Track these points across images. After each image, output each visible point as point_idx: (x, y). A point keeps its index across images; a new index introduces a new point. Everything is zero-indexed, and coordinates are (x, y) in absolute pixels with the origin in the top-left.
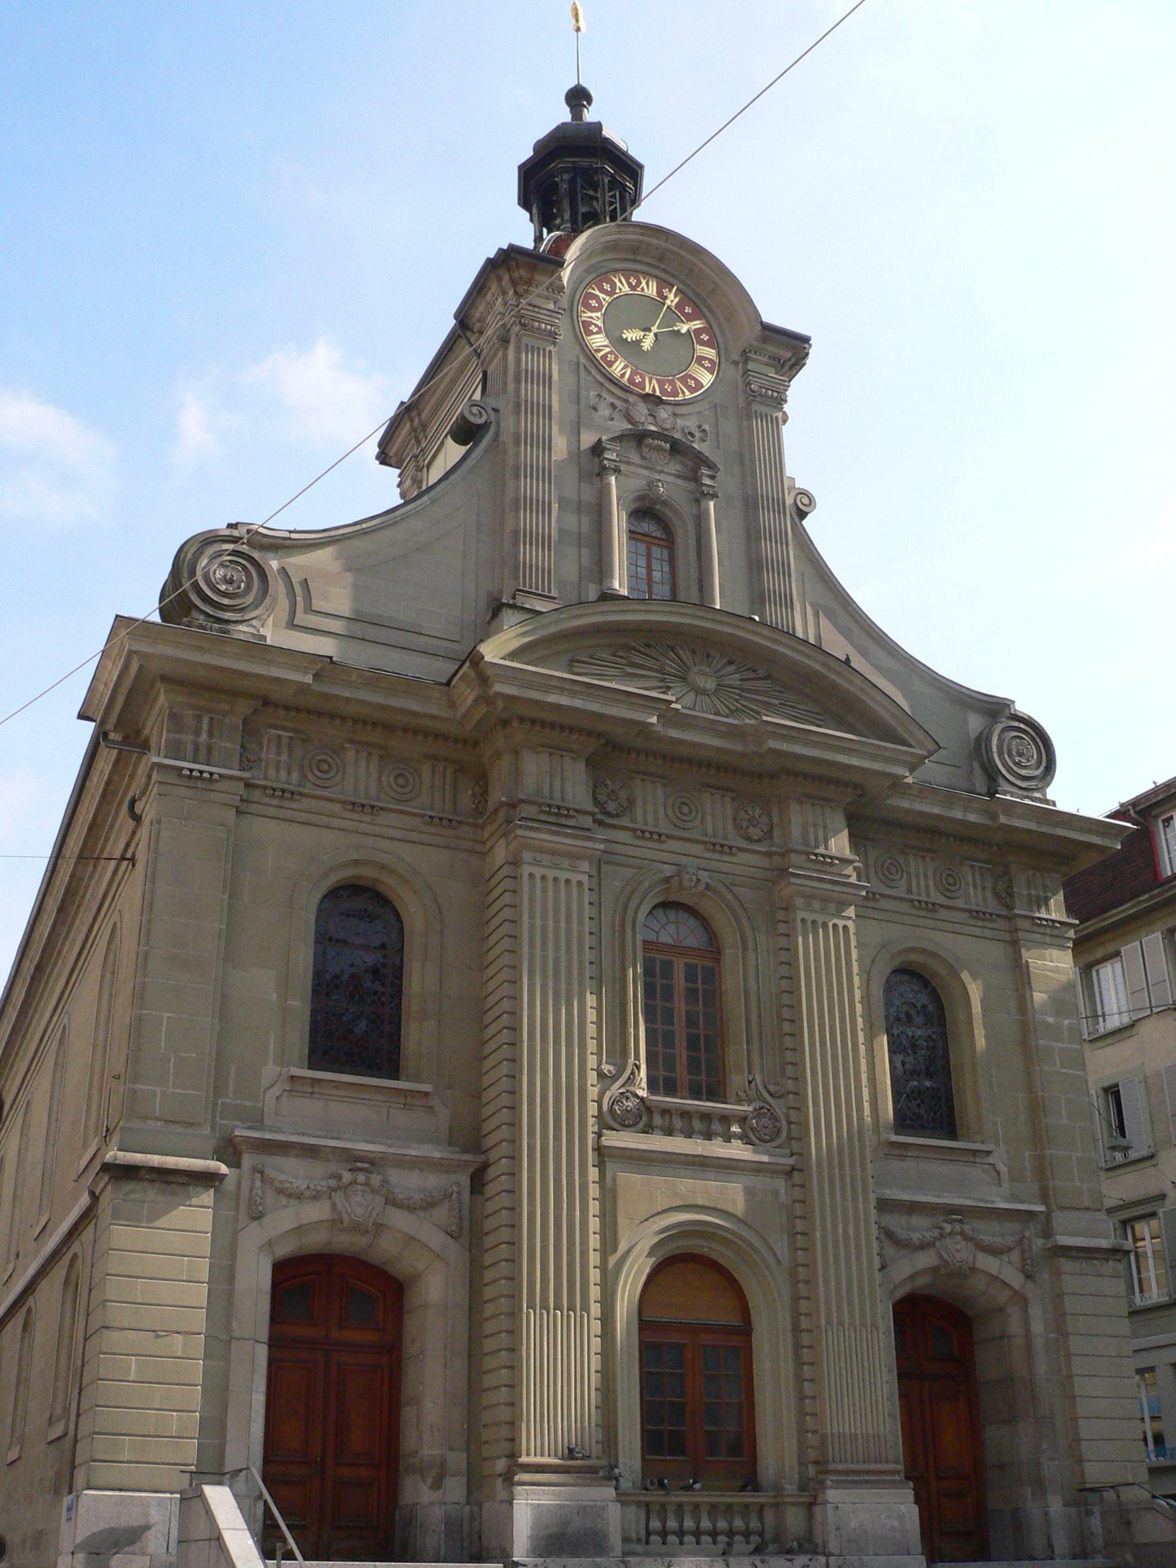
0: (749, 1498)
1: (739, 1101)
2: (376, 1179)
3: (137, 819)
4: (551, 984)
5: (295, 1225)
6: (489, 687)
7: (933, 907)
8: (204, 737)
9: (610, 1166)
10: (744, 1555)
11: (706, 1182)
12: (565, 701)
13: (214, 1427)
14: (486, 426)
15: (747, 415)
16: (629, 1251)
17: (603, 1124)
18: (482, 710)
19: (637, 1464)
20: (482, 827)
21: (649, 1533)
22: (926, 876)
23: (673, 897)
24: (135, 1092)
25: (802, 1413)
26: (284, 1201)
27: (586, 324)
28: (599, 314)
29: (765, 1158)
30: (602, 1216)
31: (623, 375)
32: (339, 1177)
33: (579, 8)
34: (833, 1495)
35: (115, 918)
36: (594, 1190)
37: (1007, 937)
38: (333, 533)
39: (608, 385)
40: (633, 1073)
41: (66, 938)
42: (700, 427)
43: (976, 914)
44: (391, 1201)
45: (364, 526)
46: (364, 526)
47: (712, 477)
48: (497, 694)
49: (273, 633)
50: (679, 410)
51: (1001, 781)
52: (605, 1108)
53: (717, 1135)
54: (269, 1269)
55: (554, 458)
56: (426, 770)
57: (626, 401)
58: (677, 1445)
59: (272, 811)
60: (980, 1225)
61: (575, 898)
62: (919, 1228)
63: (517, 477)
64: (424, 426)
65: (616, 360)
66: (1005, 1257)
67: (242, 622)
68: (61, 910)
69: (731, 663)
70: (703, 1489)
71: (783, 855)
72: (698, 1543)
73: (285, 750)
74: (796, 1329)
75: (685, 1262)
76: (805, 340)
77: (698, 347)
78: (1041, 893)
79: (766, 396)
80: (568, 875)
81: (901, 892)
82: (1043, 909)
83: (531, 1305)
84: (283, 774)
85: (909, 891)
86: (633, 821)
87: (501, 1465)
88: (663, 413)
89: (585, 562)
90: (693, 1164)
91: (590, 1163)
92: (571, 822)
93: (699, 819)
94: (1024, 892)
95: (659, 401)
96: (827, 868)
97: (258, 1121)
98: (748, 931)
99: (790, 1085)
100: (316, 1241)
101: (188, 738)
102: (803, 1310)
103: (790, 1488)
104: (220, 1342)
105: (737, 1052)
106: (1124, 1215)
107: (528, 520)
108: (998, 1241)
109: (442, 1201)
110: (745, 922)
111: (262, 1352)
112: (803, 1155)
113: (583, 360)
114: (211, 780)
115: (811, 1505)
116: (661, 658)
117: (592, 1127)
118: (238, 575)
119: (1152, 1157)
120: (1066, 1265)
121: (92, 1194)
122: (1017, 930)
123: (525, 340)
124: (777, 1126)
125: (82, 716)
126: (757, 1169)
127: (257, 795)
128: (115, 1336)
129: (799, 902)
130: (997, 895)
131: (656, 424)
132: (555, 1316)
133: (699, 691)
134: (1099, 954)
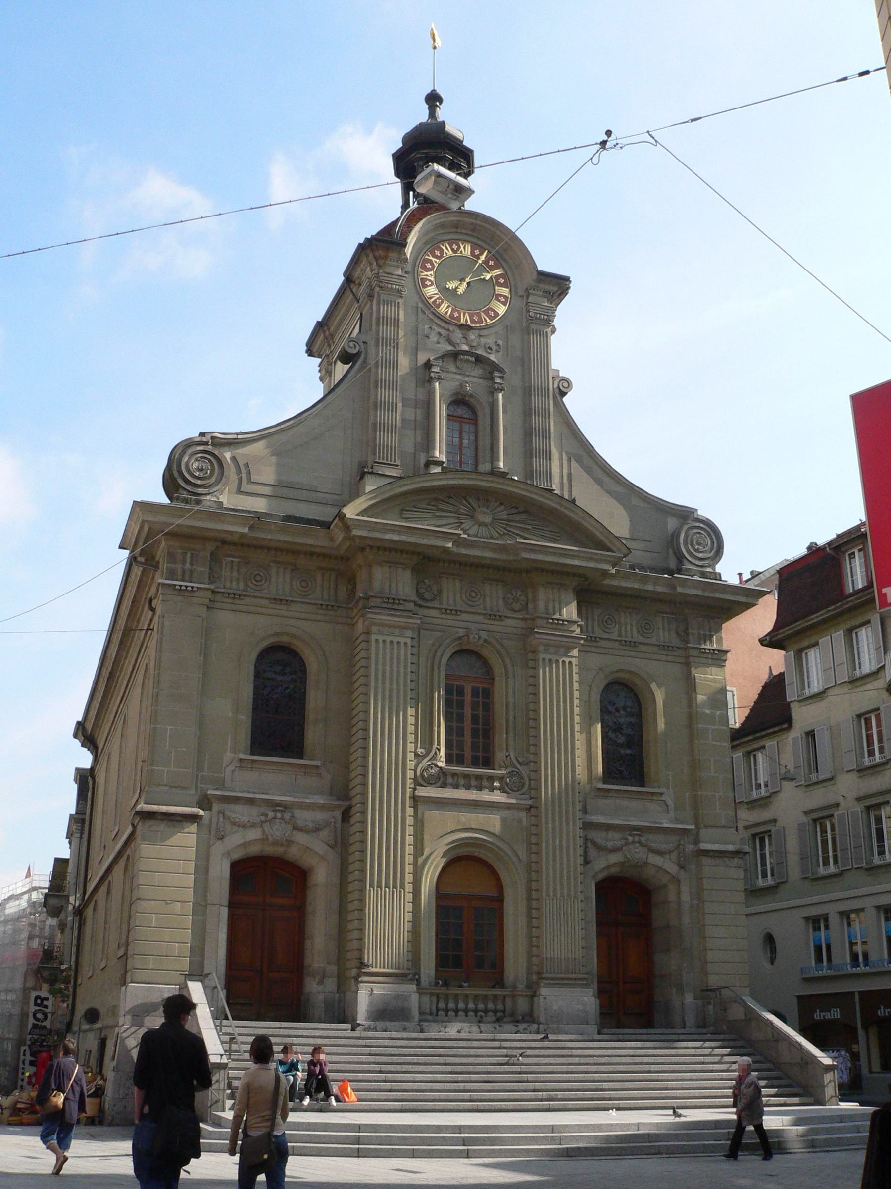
0: (498, 992)
1: (500, 768)
2: (287, 816)
3: (153, 610)
4: (387, 703)
5: (242, 841)
6: (351, 531)
7: (633, 644)
8: (188, 565)
9: (420, 807)
10: (489, 1022)
11: (481, 814)
12: (395, 537)
13: (198, 951)
14: (358, 354)
15: (527, 332)
16: (430, 855)
17: (417, 783)
18: (348, 544)
19: (433, 973)
20: (352, 609)
21: (438, 1010)
22: (631, 625)
23: (467, 647)
24: (153, 771)
25: (531, 945)
26: (236, 828)
27: (424, 280)
28: (432, 273)
29: (514, 801)
30: (415, 836)
31: (446, 313)
32: (267, 816)
33: (435, 32)
34: (544, 991)
35: (147, 661)
36: (410, 821)
37: (682, 660)
38: (263, 433)
39: (436, 320)
40: (435, 753)
41: (126, 658)
42: (496, 342)
43: (665, 647)
44: (296, 828)
45: (282, 426)
46: (282, 426)
47: (502, 378)
48: (355, 536)
49: (227, 498)
50: (483, 333)
51: (685, 562)
52: (418, 774)
53: (486, 787)
54: (229, 865)
55: (399, 373)
56: (319, 578)
57: (448, 330)
58: (458, 962)
59: (228, 606)
60: (651, 837)
61: (403, 652)
62: (613, 839)
63: (377, 388)
64: (332, 336)
65: (442, 302)
66: (668, 856)
67: (209, 494)
68: (121, 643)
69: (502, 504)
70: (468, 987)
71: (533, 619)
72: (466, 1016)
73: (235, 568)
74: (529, 899)
75: (464, 860)
76: (567, 279)
77: (497, 288)
78: (708, 633)
79: (539, 319)
80: (399, 639)
81: (615, 636)
82: (708, 643)
83: (372, 886)
84: (234, 583)
85: (620, 635)
86: (441, 604)
87: (354, 972)
88: (472, 336)
89: (419, 439)
90: (470, 805)
91: (408, 805)
92: (401, 607)
93: (481, 601)
94: (695, 631)
95: (471, 328)
96: (560, 627)
97: (221, 785)
98: (509, 666)
99: (532, 758)
100: (254, 850)
101: (178, 567)
102: (533, 887)
103: (521, 987)
104: (201, 906)
105: (500, 738)
106: (815, 816)
107: (382, 416)
108: (663, 847)
109: (325, 827)
110: (508, 661)
111: (225, 911)
112: (537, 798)
113: (420, 305)
114: (192, 591)
115: (532, 997)
116: (458, 505)
117: (409, 782)
118: (206, 465)
119: (832, 779)
120: (705, 860)
121: (133, 825)
122: (689, 656)
123: (382, 297)
124: (523, 783)
125: (121, 547)
126: (509, 807)
127: (219, 597)
128: (144, 904)
129: (541, 648)
130: (678, 634)
131: (467, 344)
132: (385, 892)
133: (481, 524)
134: (806, 643)
